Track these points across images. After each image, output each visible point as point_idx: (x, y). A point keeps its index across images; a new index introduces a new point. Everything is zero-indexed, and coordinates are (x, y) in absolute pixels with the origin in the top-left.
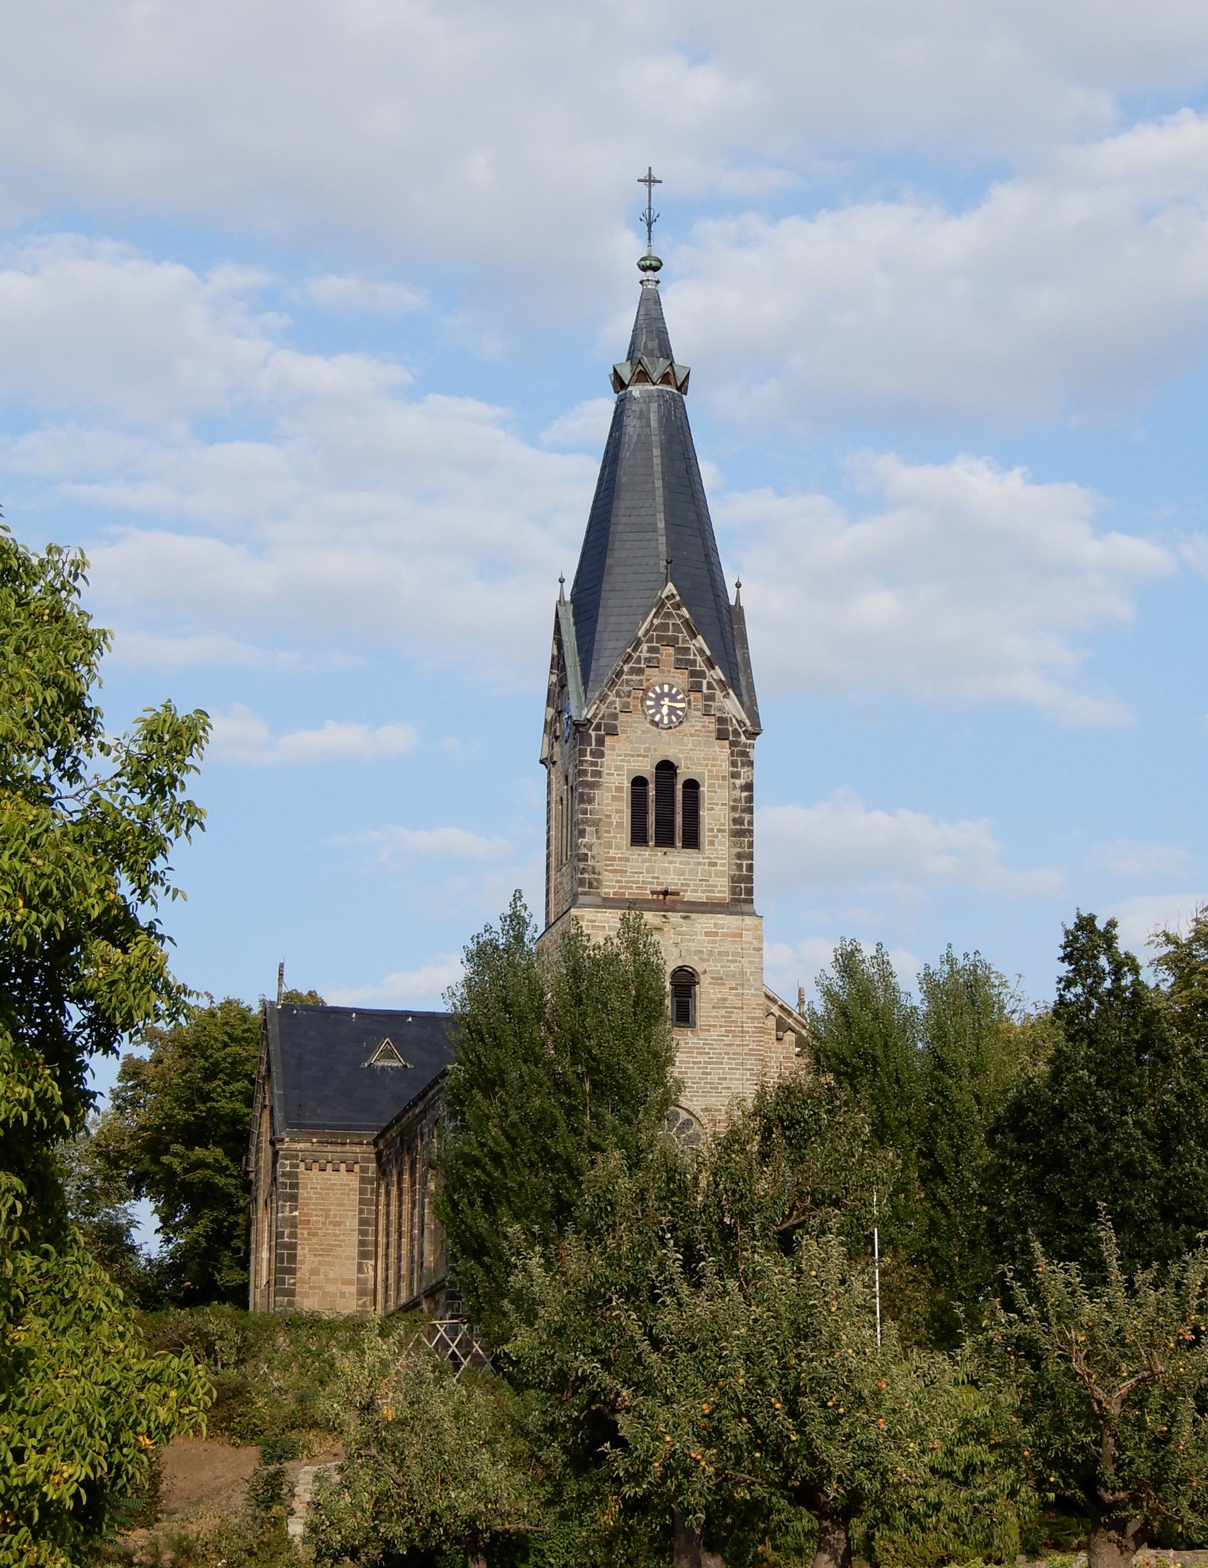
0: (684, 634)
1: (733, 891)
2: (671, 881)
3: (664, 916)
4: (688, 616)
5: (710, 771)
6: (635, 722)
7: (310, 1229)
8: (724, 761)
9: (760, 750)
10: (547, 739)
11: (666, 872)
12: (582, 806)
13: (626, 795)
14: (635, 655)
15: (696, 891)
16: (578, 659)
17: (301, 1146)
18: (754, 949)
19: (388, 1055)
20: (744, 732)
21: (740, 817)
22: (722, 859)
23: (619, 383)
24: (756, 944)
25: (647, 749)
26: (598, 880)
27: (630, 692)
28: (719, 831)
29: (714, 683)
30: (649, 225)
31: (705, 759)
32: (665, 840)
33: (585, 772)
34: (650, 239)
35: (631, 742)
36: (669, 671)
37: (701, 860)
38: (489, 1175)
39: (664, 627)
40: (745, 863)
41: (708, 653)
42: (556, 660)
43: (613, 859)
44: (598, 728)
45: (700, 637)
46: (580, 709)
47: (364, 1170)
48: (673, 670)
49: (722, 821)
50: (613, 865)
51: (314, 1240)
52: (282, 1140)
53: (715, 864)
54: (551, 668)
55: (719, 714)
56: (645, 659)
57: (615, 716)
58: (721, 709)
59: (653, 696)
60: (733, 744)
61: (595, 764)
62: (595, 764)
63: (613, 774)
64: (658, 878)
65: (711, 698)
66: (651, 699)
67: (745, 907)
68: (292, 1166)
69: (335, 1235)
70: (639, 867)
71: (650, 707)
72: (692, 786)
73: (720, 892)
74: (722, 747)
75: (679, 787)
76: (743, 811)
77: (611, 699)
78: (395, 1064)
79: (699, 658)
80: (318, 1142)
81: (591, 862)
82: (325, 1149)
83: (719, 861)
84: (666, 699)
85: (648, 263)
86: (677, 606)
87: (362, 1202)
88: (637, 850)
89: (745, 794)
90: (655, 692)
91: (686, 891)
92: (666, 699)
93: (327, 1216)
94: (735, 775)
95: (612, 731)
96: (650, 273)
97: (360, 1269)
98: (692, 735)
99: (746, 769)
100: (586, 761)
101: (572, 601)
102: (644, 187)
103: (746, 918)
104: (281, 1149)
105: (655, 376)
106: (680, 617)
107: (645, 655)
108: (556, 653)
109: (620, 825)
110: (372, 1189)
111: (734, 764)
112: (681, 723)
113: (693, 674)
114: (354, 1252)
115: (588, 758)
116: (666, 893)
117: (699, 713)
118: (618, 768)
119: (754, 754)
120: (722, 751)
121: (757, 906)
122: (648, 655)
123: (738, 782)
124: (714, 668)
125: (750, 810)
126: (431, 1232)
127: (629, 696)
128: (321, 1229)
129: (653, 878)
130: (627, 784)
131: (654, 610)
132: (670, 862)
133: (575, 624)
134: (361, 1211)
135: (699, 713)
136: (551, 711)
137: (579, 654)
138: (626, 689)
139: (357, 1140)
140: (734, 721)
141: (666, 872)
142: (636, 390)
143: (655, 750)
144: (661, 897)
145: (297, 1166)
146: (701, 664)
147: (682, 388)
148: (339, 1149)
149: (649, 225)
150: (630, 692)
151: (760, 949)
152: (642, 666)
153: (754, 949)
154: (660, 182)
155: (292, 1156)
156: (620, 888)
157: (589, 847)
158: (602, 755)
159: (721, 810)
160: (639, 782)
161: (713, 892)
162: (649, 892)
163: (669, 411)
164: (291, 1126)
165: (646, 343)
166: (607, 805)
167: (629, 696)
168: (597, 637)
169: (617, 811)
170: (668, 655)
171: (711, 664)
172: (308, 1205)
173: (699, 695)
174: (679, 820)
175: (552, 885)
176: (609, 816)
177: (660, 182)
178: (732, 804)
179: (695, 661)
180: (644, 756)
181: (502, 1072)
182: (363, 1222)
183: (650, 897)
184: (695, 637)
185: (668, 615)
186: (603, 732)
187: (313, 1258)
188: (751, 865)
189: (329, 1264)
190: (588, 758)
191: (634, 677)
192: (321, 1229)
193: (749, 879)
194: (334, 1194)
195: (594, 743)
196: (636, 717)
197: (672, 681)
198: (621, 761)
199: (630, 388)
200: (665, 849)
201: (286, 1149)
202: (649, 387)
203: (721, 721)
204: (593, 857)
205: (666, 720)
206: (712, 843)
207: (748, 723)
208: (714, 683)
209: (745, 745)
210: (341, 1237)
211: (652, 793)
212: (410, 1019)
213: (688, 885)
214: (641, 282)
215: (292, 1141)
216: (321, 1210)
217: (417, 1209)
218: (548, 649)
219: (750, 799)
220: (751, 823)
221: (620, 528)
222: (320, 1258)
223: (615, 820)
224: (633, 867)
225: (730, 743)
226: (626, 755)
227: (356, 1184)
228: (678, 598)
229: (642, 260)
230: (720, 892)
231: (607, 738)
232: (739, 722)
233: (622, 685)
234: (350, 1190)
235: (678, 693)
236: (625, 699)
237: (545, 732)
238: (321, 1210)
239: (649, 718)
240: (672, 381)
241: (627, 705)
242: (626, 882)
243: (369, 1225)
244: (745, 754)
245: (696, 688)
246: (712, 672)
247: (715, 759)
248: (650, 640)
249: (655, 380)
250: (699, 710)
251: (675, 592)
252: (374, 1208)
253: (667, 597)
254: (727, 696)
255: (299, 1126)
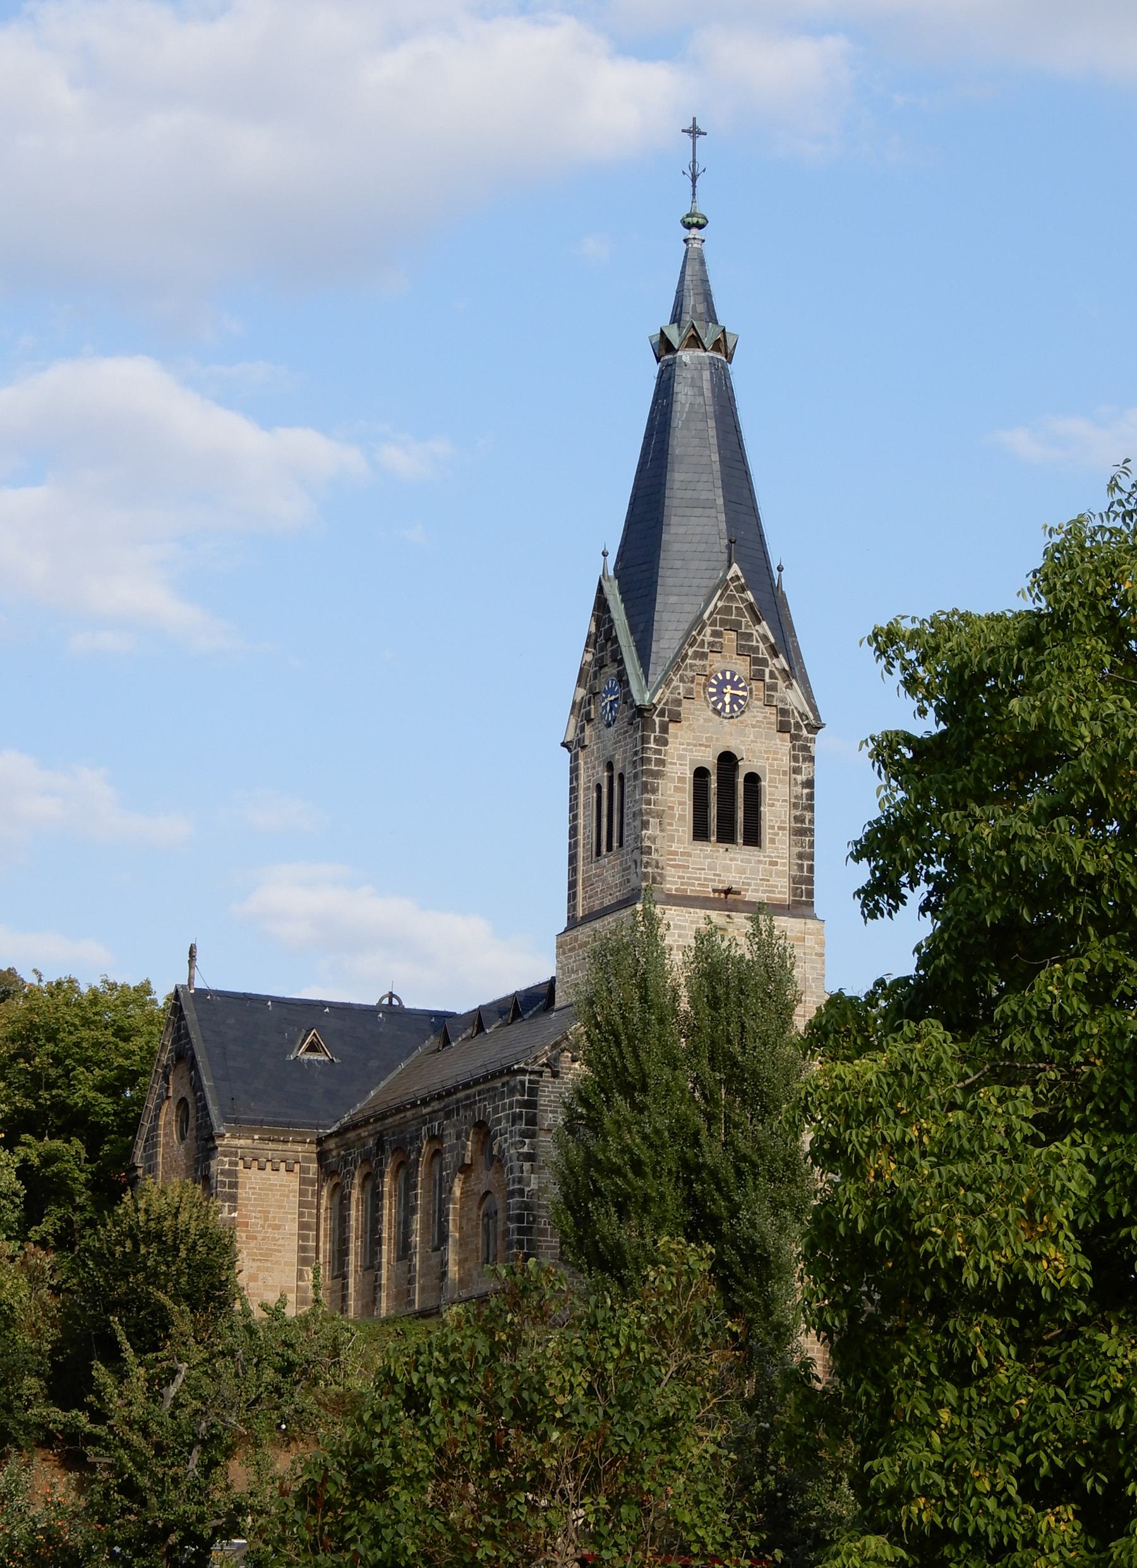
0: (747, 619)
1: (794, 892)
2: (732, 879)
3: (728, 916)
4: (752, 600)
5: (771, 765)
6: (698, 710)
7: (248, 1231)
8: (784, 755)
9: (821, 744)
10: (573, 721)
11: (727, 869)
12: (645, 796)
13: (689, 786)
14: (699, 639)
15: (757, 891)
16: (631, 639)
17: (242, 1142)
18: (816, 954)
19: (312, 1048)
20: (806, 725)
21: (801, 815)
22: (783, 858)
23: (664, 346)
24: (818, 949)
25: (709, 739)
26: (661, 875)
27: (693, 677)
28: (780, 828)
29: (776, 672)
30: (694, 179)
31: (766, 752)
32: (726, 836)
33: (649, 760)
34: (694, 194)
35: (693, 730)
36: (731, 657)
37: (762, 858)
38: (629, 1183)
39: (727, 610)
40: (806, 863)
41: (773, 640)
42: (593, 638)
43: (675, 853)
44: (662, 714)
45: (764, 623)
46: (643, 693)
47: (304, 1170)
48: (735, 656)
49: (783, 818)
50: (674, 860)
51: (253, 1244)
52: (222, 1136)
53: (776, 864)
54: (587, 645)
55: (780, 706)
56: (709, 643)
57: (678, 703)
58: (783, 700)
59: (715, 683)
60: (794, 738)
61: (658, 752)
62: (658, 752)
63: (675, 764)
64: (719, 875)
65: (773, 688)
66: (712, 685)
67: (805, 910)
68: (231, 1163)
69: (274, 1239)
70: (701, 863)
71: (712, 695)
72: (753, 779)
73: (780, 893)
74: (783, 740)
75: (741, 780)
76: (804, 809)
77: (674, 684)
78: (322, 1057)
79: (761, 645)
80: (260, 1139)
81: (654, 856)
82: (266, 1147)
83: (779, 861)
84: (729, 687)
85: (695, 220)
86: (742, 589)
87: (301, 1205)
88: (699, 845)
89: (806, 791)
90: (716, 678)
91: (747, 890)
92: (729, 687)
93: (266, 1219)
94: (797, 771)
95: (676, 719)
96: (694, 231)
97: (300, 1276)
98: (753, 726)
99: (807, 764)
100: (650, 749)
101: (617, 576)
102: (687, 138)
103: (808, 921)
104: (221, 1145)
105: (707, 342)
106: (743, 600)
107: (709, 639)
108: (593, 630)
109: (682, 818)
110: (313, 1191)
111: (795, 758)
112: (743, 712)
113: (756, 661)
114: (294, 1257)
115: (652, 745)
116: (728, 891)
117: (760, 703)
118: (681, 757)
119: (816, 749)
120: (783, 744)
121: (818, 909)
122: (712, 639)
123: (800, 778)
124: (777, 657)
125: (811, 808)
126: (455, 1241)
127: (692, 682)
128: (260, 1232)
129: (715, 875)
130: (689, 775)
131: (719, 592)
132: (731, 859)
133: (623, 600)
134: (301, 1215)
135: (760, 703)
136: (582, 692)
137: (632, 634)
138: (690, 674)
139: (299, 1139)
140: (796, 714)
141: (727, 869)
142: (686, 356)
143: (717, 740)
144: (723, 895)
145: (236, 1164)
146: (763, 652)
147: (729, 357)
148: (281, 1147)
149: (694, 179)
150: (693, 677)
151: (822, 955)
152: (706, 650)
153: (816, 954)
154: (705, 134)
155: (231, 1152)
156: (682, 884)
157: (653, 839)
158: (666, 743)
159: (781, 806)
160: (701, 774)
161: (773, 892)
162: (710, 890)
163: (720, 379)
164: (228, 1121)
165: (694, 306)
166: (670, 796)
167: (692, 682)
168: (656, 618)
169: (680, 803)
170: (730, 640)
171: (775, 654)
172: (246, 1205)
173: (761, 684)
174: (740, 814)
175: (580, 877)
176: (671, 808)
177: (705, 134)
178: (793, 800)
179: (758, 647)
180: (707, 746)
181: (644, 1076)
182: (303, 1226)
183: (712, 895)
184: (759, 622)
185: (731, 598)
186: (667, 719)
187: (251, 1263)
188: (812, 866)
189: (267, 1270)
190: (652, 745)
191: (698, 662)
192: (260, 1232)
193: (810, 881)
194: (274, 1195)
195: (657, 729)
196: (699, 704)
197: (734, 668)
198: (684, 750)
199: (679, 353)
200: (727, 845)
201: (227, 1146)
202: (700, 353)
203: (783, 712)
204: (656, 850)
205: (728, 709)
206: (772, 841)
207: (811, 716)
208: (776, 672)
209: (806, 739)
210: (280, 1242)
211: (714, 785)
212: (327, 1010)
213: (749, 884)
214: (686, 241)
215: (233, 1137)
216: (260, 1212)
217: (418, 1217)
218: (583, 623)
219: (811, 797)
220: (812, 822)
221: (675, 502)
222: (259, 1264)
223: (677, 812)
224: (695, 863)
225: (791, 736)
226: (688, 744)
227: (296, 1185)
228: (743, 580)
229: (688, 216)
230: (780, 893)
231: (671, 725)
232: (801, 715)
233: (686, 669)
234: (290, 1192)
235: (740, 681)
236: (689, 685)
237: (572, 713)
238: (260, 1212)
239: (711, 706)
240: (723, 349)
241: (690, 691)
242: (689, 878)
243: (310, 1229)
244: (806, 749)
245: (758, 676)
246: (775, 661)
247: (775, 753)
248: (713, 624)
249: (706, 346)
250: (759, 700)
251: (740, 574)
252: (315, 1211)
253: (731, 579)
254: (790, 686)
255: (236, 1121)
